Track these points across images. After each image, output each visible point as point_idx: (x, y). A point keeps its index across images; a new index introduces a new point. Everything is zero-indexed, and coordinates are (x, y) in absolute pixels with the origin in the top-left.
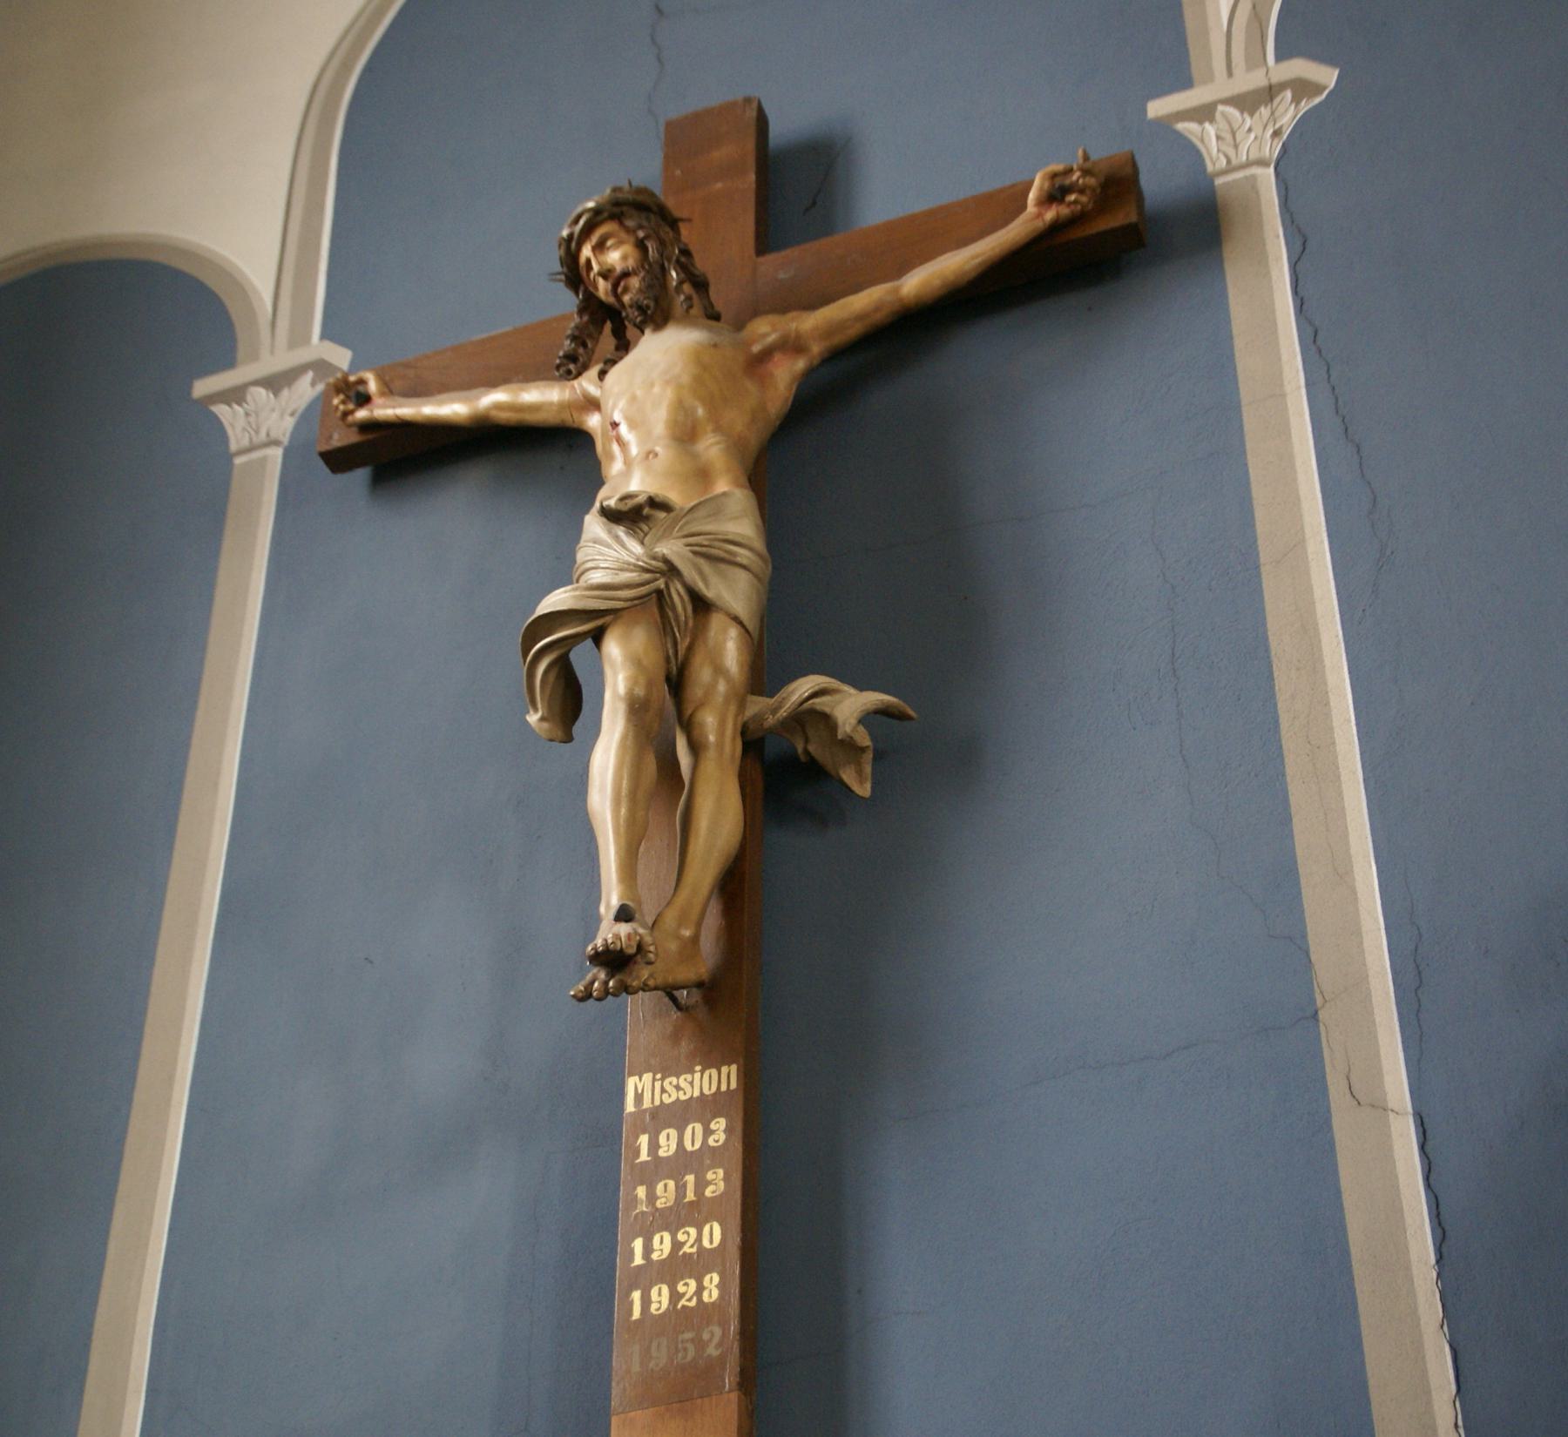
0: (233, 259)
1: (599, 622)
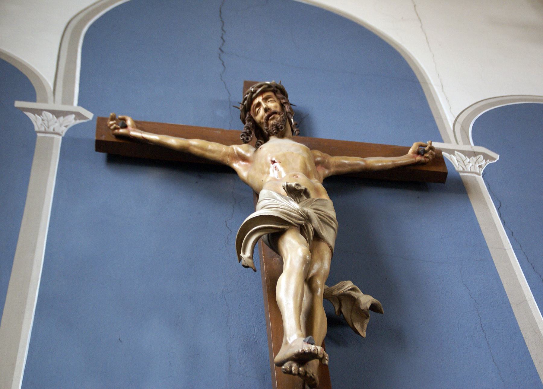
0: (33, 66)
1: (285, 227)
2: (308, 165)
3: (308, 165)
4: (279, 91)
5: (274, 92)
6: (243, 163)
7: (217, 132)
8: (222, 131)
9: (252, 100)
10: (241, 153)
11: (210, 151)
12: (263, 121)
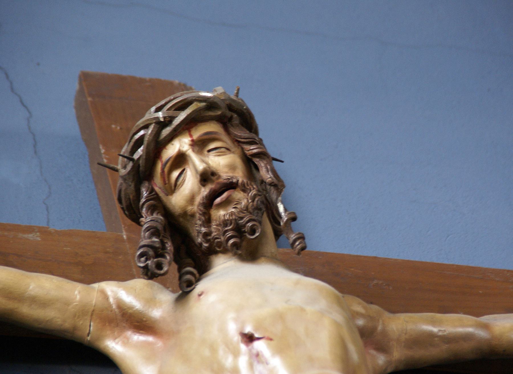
2: (352, 348)
3: (352, 348)
4: (234, 119)
5: (224, 122)
6: (138, 338)
7: (30, 236)
8: (44, 231)
9: (158, 146)
10: (131, 308)
11: (34, 300)
12: (195, 208)
